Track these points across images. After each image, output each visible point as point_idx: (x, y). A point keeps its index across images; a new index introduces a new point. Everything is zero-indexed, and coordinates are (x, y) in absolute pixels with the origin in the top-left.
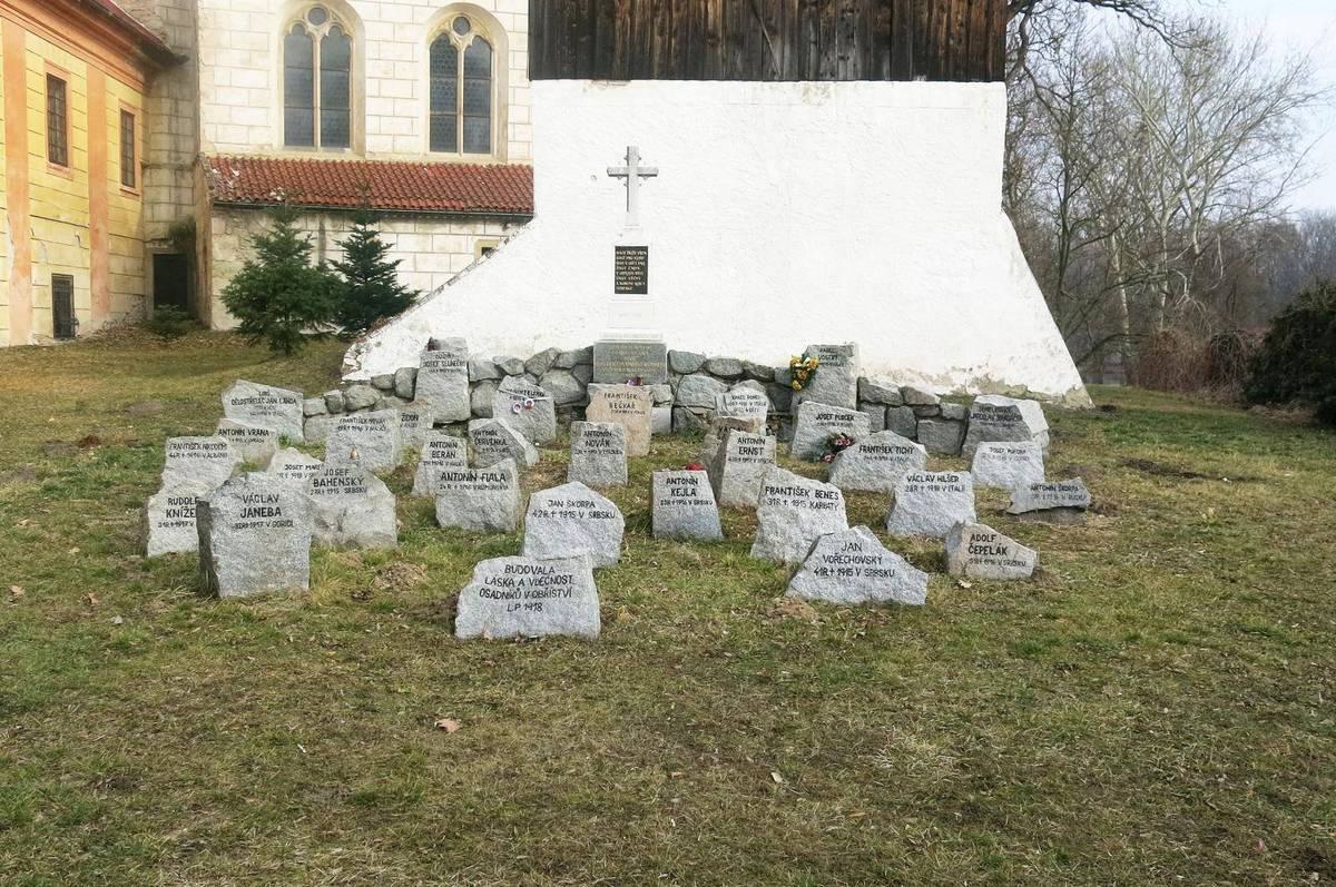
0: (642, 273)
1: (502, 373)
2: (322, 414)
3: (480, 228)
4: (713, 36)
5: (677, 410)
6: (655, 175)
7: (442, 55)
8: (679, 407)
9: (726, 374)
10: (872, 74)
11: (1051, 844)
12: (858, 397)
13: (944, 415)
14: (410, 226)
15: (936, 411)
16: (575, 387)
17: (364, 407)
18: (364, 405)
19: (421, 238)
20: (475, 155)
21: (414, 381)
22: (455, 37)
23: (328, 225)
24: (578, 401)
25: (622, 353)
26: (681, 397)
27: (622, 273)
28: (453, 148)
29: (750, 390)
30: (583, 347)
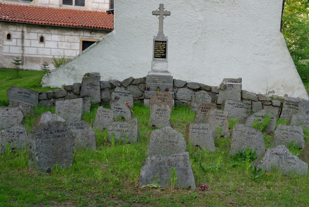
0: (164, 51)
1: (200, 89)
2: (46, 100)
3: (82, 34)
6: (170, 15)
8: (177, 100)
9: (194, 88)
11: (18, 180)
12: (242, 97)
13: (273, 104)
14: (56, 32)
15: (270, 103)
16: (139, 92)
17: (61, 97)
18: (61, 96)
19: (60, 36)
20: (79, 7)
21: (80, 88)
23: (25, 30)
24: (140, 97)
25: (157, 80)
26: (178, 96)
27: (157, 51)
28: (71, 4)
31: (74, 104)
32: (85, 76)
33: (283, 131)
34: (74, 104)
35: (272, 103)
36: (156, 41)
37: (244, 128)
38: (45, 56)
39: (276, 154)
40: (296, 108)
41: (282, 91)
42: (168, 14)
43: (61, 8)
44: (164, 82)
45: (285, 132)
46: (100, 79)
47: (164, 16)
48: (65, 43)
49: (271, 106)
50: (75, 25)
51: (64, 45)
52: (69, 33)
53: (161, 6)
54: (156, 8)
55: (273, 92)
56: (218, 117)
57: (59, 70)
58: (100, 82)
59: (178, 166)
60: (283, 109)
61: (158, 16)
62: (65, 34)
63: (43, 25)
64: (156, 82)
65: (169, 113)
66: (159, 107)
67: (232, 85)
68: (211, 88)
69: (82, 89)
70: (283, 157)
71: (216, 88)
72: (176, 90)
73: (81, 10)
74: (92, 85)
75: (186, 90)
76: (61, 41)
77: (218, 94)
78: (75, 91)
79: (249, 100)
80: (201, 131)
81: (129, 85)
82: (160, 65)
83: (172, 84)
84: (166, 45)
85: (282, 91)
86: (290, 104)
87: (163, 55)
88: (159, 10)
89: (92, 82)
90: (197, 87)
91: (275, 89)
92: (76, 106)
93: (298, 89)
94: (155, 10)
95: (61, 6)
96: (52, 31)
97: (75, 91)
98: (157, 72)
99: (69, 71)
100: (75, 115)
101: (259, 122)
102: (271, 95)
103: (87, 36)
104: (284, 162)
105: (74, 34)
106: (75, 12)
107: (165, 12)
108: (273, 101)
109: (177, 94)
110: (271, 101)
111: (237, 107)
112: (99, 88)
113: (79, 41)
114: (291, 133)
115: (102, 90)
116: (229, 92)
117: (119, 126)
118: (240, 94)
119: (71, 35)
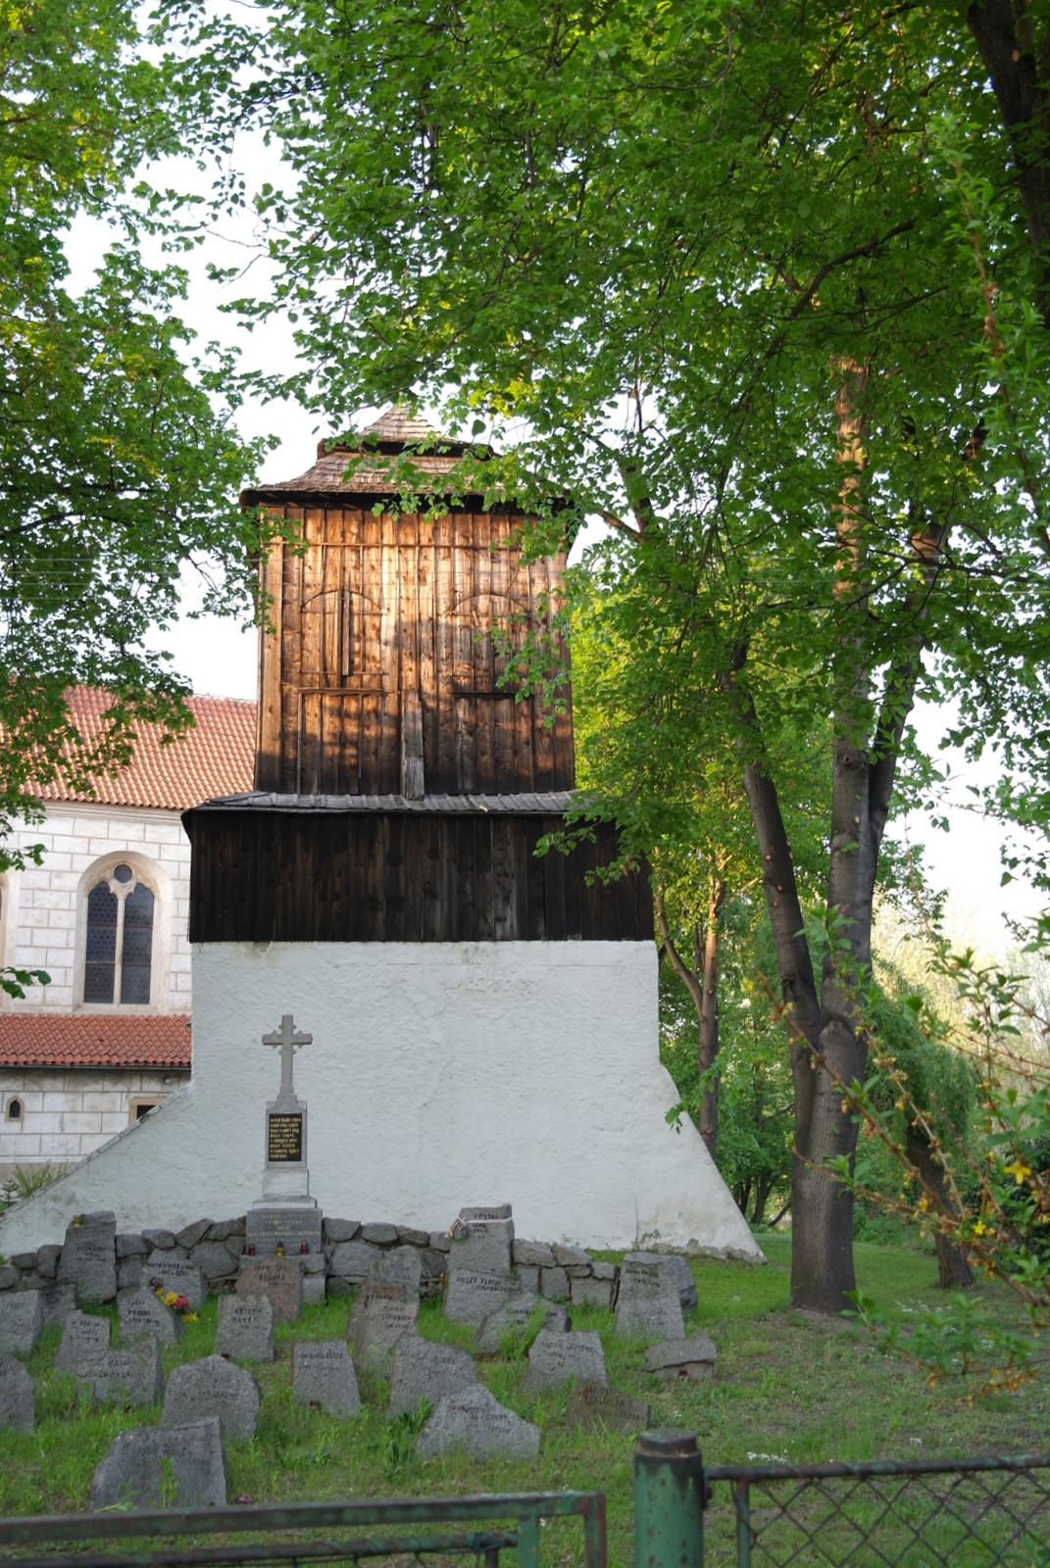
1: (398, 1242)
3: (136, 1085)
4: (373, 899)
5: (332, 1280)
7: (100, 903)
9: (381, 1240)
10: (527, 933)
14: (59, 1084)
15: (588, 1272)
20: (134, 1006)
21: (58, 1258)
22: (114, 886)
25: (276, 1222)
28: (109, 999)
29: (410, 1255)
30: (236, 1216)
31: (15, 1306)
32: (73, 1222)
33: (552, 1350)
34: (15, 1306)
35: (592, 1270)
36: (272, 1116)
37: (423, 1348)
38: (22, 1160)
39: (463, 1408)
40: (654, 1280)
41: (681, 1231)
42: (305, 1040)
43: (78, 1014)
44: (294, 1228)
45: (557, 1350)
46: (114, 1228)
47: (295, 1047)
48: (85, 1116)
49: (590, 1280)
50: (115, 1060)
51: (81, 1123)
52: (98, 1087)
53: (288, 1021)
54: (274, 1027)
55: (657, 1234)
56: (390, 1321)
57: (31, 1204)
58: (116, 1239)
59: (190, 1453)
60: (622, 1286)
61: (279, 1047)
62: (87, 1089)
63: (20, 1069)
64: (274, 1228)
65: (269, 1318)
66: (242, 1303)
67: (484, 1225)
68: (428, 1237)
69: (62, 1263)
70: (480, 1414)
71: (442, 1235)
72: (328, 1249)
73: (137, 1015)
74: (92, 1249)
75: (358, 1247)
76: (73, 1112)
77: (448, 1252)
78: (43, 1268)
79: (534, 1265)
80: (325, 1362)
81: (200, 1242)
82: (287, 1182)
83: (319, 1233)
84: (300, 1125)
85: (681, 1231)
86: (636, 1272)
87: (292, 1151)
88: (280, 1032)
89: (90, 1239)
90: (391, 1237)
91: (660, 1227)
92: (19, 1312)
93: (726, 1220)
94: (270, 1032)
95: (77, 1007)
96: (47, 1084)
97: (43, 1268)
98: (275, 1200)
99: (58, 1206)
100: (17, 1338)
101: (518, 1327)
102: (650, 1243)
103: (148, 1089)
104: (481, 1428)
105: (111, 1088)
106: (120, 1022)
107: (297, 1036)
108: (595, 1265)
109: (335, 1260)
110: (589, 1266)
111: (483, 1288)
112: (111, 1255)
113: (126, 1108)
114: (572, 1352)
115: (120, 1260)
116: (476, 1245)
117: (106, 1361)
118: (505, 1251)
119: (103, 1092)
